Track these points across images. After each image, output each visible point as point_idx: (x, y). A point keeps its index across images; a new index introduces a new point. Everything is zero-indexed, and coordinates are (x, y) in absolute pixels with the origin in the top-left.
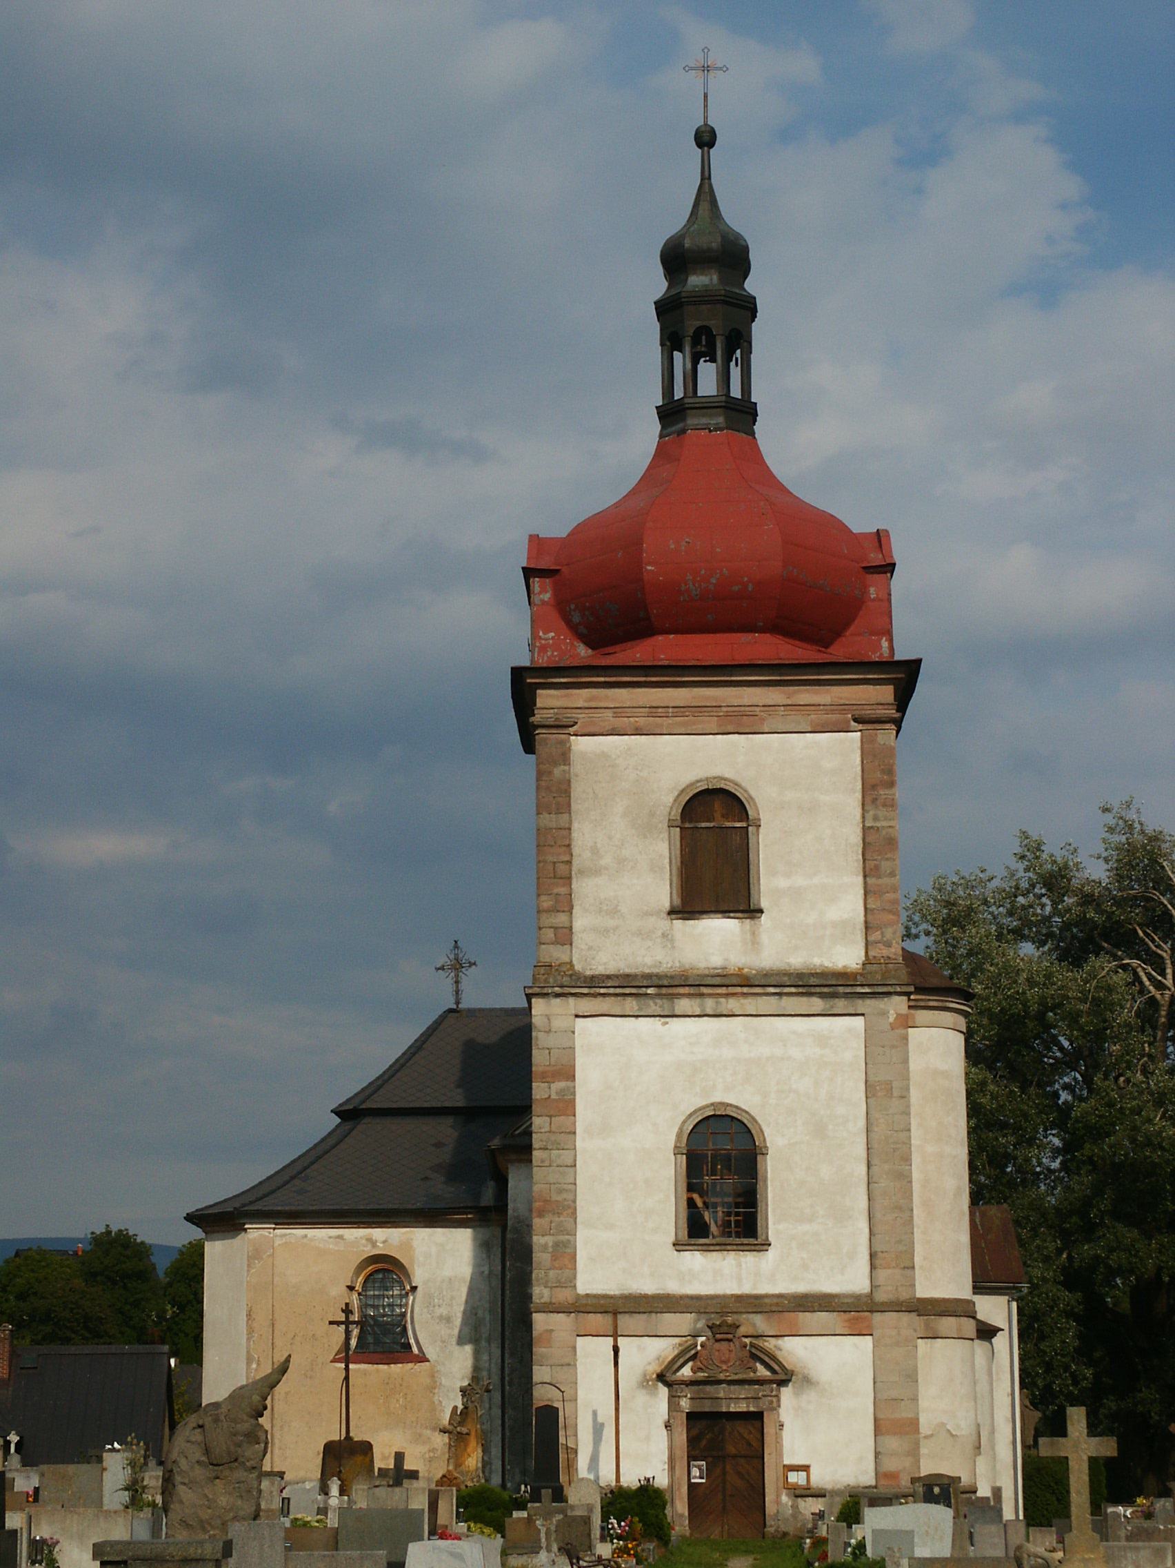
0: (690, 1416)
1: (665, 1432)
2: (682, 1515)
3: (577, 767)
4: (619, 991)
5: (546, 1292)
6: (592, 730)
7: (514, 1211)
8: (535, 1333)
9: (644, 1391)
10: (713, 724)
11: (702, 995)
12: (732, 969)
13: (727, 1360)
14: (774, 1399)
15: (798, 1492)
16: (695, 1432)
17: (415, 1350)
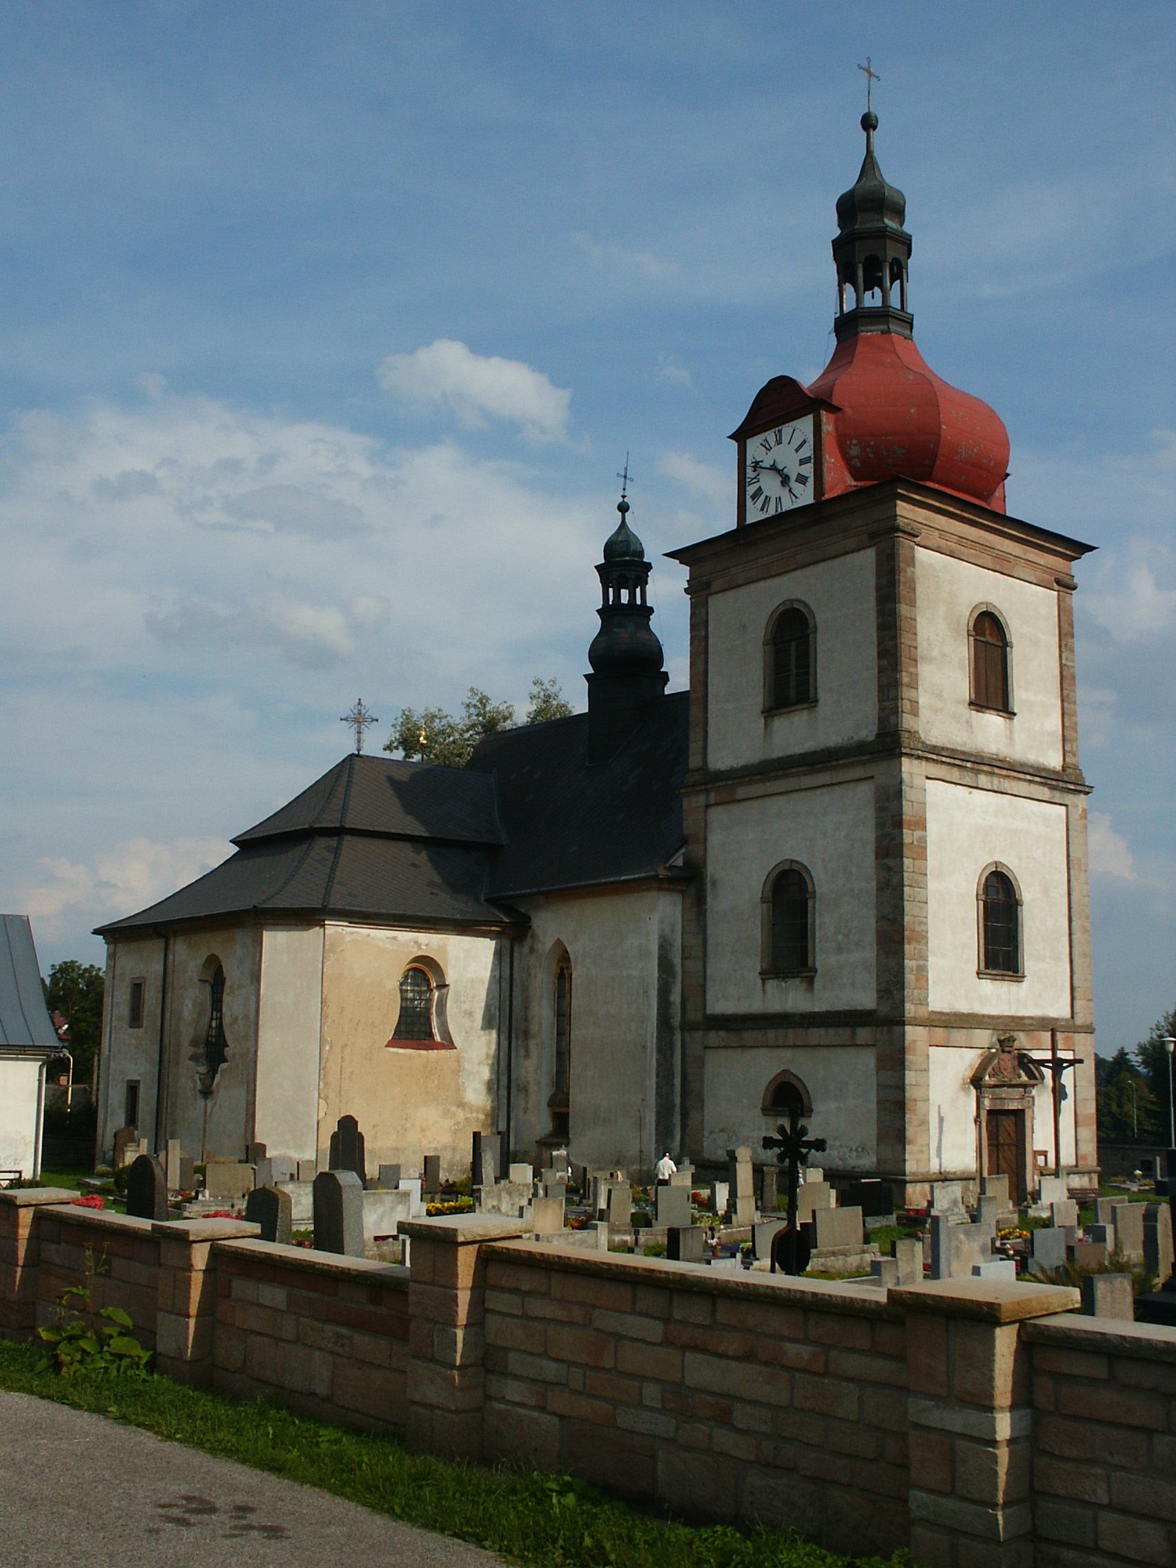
0: (990, 1112)
3: (919, 571)
4: (948, 760)
5: (913, 1007)
6: (929, 544)
8: (907, 1043)
10: (988, 561)
11: (993, 774)
17: (438, 1038)
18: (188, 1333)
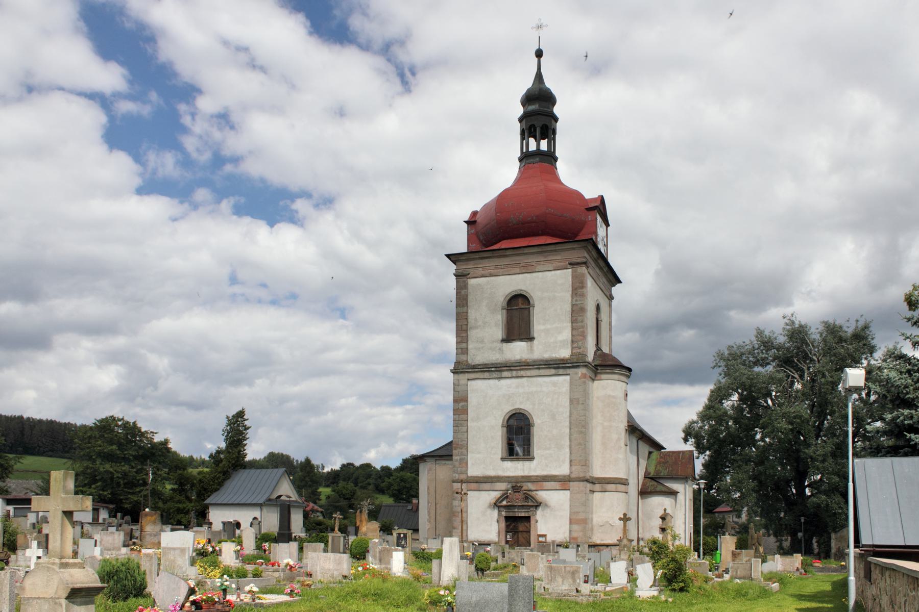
13: (518, 499)
18: (848, 473)
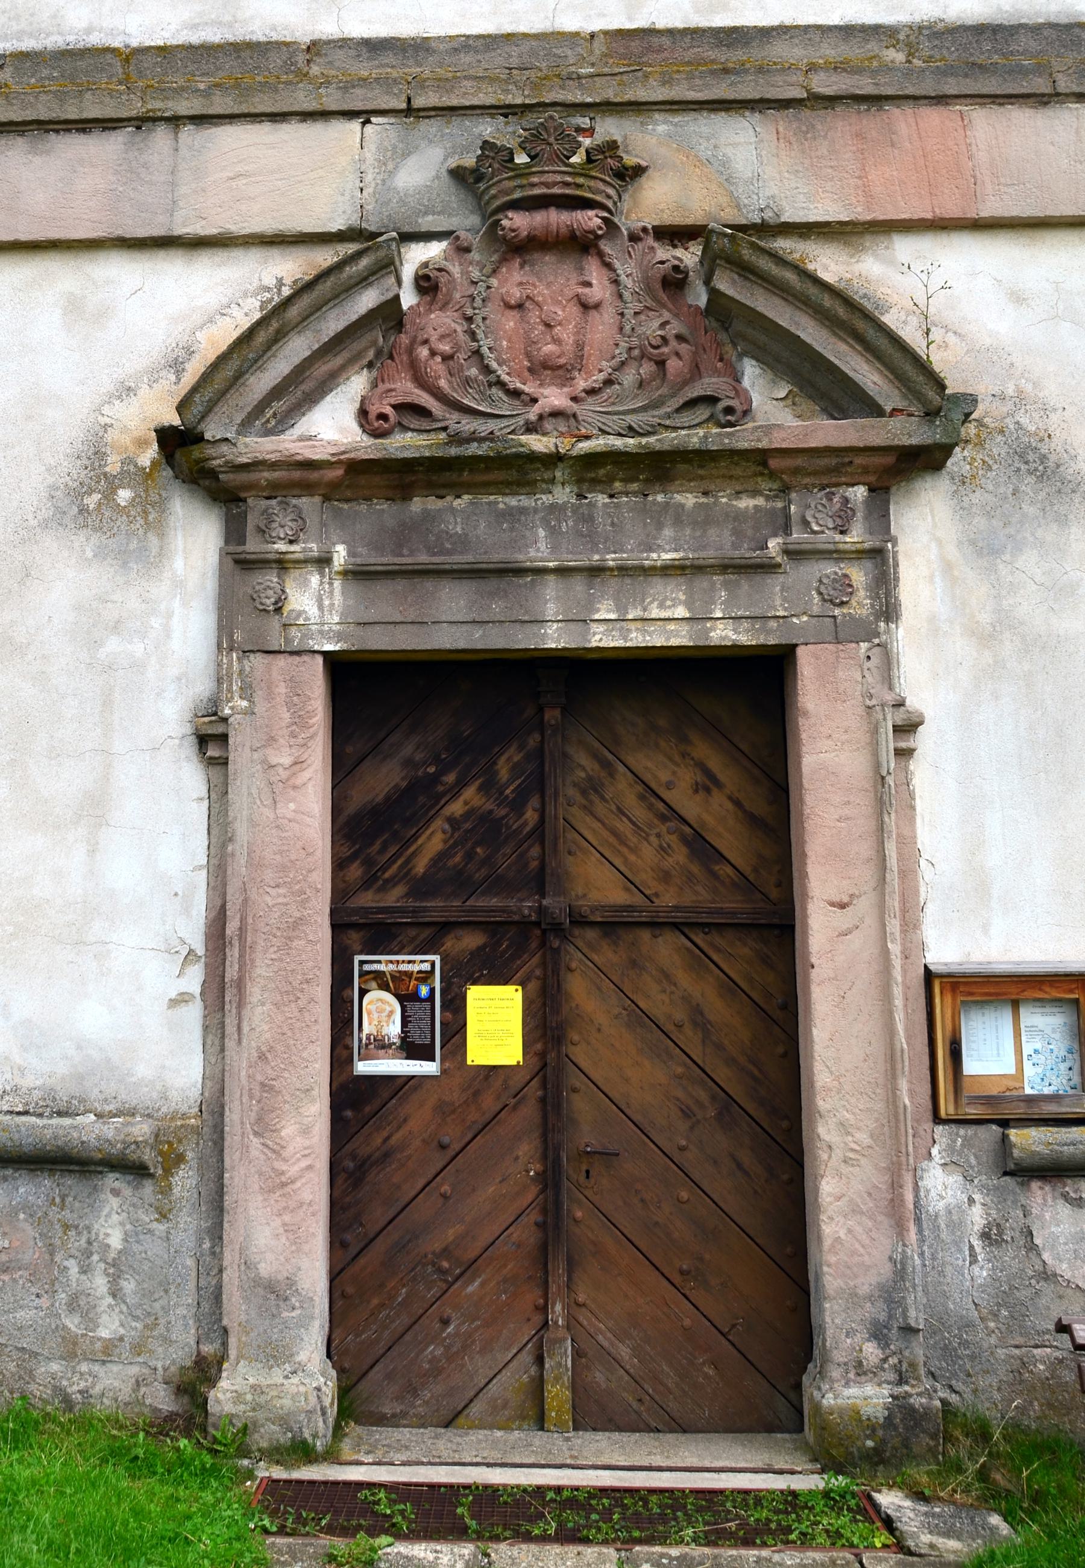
0: (346, 673)
1: (192, 778)
2: (276, 1292)
7: (891, 1329)
9: (86, 543)
12: (422, 244)
13: (572, 344)
14: (859, 575)
15: (1029, 1140)
16: (382, 779)
